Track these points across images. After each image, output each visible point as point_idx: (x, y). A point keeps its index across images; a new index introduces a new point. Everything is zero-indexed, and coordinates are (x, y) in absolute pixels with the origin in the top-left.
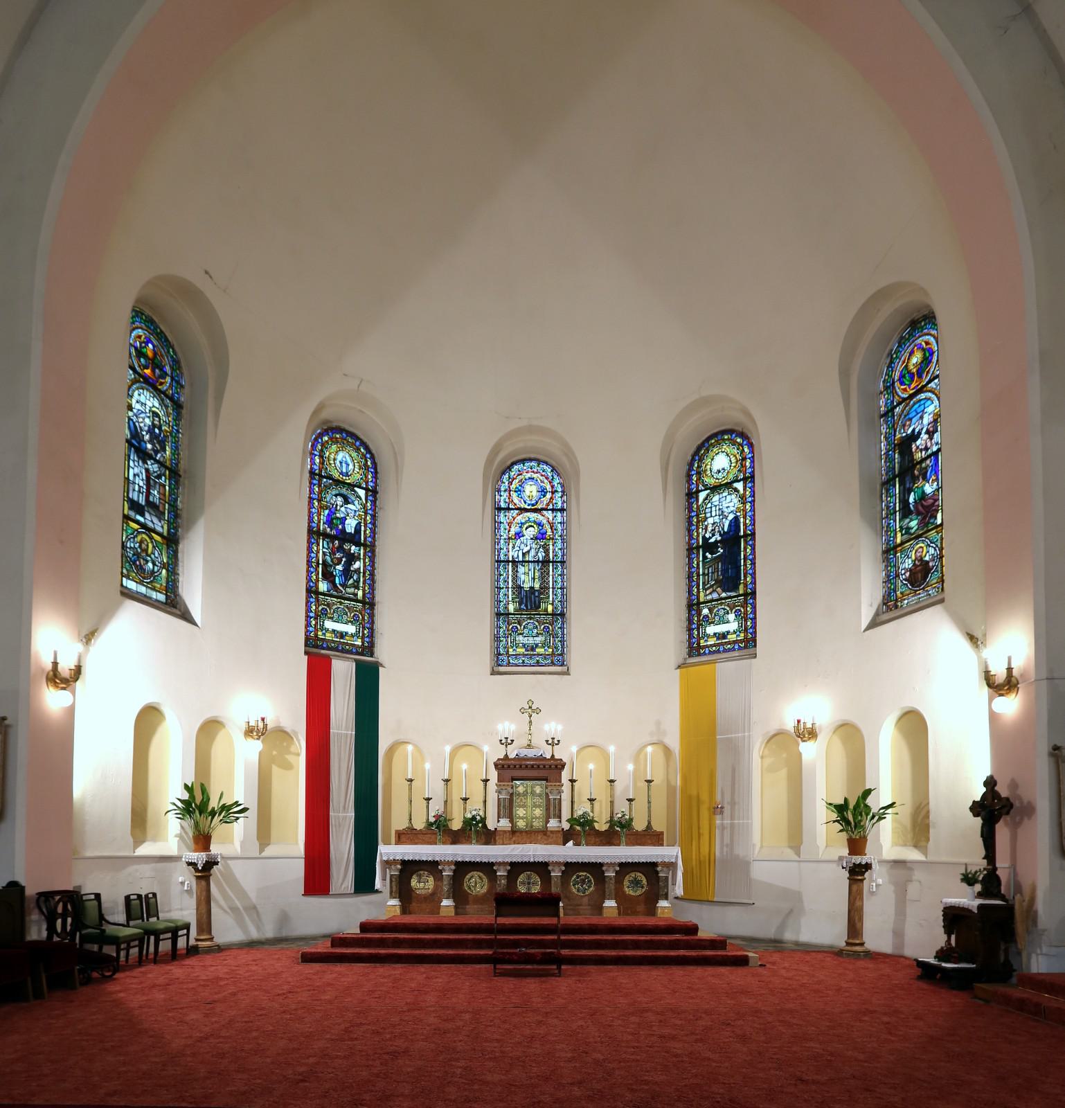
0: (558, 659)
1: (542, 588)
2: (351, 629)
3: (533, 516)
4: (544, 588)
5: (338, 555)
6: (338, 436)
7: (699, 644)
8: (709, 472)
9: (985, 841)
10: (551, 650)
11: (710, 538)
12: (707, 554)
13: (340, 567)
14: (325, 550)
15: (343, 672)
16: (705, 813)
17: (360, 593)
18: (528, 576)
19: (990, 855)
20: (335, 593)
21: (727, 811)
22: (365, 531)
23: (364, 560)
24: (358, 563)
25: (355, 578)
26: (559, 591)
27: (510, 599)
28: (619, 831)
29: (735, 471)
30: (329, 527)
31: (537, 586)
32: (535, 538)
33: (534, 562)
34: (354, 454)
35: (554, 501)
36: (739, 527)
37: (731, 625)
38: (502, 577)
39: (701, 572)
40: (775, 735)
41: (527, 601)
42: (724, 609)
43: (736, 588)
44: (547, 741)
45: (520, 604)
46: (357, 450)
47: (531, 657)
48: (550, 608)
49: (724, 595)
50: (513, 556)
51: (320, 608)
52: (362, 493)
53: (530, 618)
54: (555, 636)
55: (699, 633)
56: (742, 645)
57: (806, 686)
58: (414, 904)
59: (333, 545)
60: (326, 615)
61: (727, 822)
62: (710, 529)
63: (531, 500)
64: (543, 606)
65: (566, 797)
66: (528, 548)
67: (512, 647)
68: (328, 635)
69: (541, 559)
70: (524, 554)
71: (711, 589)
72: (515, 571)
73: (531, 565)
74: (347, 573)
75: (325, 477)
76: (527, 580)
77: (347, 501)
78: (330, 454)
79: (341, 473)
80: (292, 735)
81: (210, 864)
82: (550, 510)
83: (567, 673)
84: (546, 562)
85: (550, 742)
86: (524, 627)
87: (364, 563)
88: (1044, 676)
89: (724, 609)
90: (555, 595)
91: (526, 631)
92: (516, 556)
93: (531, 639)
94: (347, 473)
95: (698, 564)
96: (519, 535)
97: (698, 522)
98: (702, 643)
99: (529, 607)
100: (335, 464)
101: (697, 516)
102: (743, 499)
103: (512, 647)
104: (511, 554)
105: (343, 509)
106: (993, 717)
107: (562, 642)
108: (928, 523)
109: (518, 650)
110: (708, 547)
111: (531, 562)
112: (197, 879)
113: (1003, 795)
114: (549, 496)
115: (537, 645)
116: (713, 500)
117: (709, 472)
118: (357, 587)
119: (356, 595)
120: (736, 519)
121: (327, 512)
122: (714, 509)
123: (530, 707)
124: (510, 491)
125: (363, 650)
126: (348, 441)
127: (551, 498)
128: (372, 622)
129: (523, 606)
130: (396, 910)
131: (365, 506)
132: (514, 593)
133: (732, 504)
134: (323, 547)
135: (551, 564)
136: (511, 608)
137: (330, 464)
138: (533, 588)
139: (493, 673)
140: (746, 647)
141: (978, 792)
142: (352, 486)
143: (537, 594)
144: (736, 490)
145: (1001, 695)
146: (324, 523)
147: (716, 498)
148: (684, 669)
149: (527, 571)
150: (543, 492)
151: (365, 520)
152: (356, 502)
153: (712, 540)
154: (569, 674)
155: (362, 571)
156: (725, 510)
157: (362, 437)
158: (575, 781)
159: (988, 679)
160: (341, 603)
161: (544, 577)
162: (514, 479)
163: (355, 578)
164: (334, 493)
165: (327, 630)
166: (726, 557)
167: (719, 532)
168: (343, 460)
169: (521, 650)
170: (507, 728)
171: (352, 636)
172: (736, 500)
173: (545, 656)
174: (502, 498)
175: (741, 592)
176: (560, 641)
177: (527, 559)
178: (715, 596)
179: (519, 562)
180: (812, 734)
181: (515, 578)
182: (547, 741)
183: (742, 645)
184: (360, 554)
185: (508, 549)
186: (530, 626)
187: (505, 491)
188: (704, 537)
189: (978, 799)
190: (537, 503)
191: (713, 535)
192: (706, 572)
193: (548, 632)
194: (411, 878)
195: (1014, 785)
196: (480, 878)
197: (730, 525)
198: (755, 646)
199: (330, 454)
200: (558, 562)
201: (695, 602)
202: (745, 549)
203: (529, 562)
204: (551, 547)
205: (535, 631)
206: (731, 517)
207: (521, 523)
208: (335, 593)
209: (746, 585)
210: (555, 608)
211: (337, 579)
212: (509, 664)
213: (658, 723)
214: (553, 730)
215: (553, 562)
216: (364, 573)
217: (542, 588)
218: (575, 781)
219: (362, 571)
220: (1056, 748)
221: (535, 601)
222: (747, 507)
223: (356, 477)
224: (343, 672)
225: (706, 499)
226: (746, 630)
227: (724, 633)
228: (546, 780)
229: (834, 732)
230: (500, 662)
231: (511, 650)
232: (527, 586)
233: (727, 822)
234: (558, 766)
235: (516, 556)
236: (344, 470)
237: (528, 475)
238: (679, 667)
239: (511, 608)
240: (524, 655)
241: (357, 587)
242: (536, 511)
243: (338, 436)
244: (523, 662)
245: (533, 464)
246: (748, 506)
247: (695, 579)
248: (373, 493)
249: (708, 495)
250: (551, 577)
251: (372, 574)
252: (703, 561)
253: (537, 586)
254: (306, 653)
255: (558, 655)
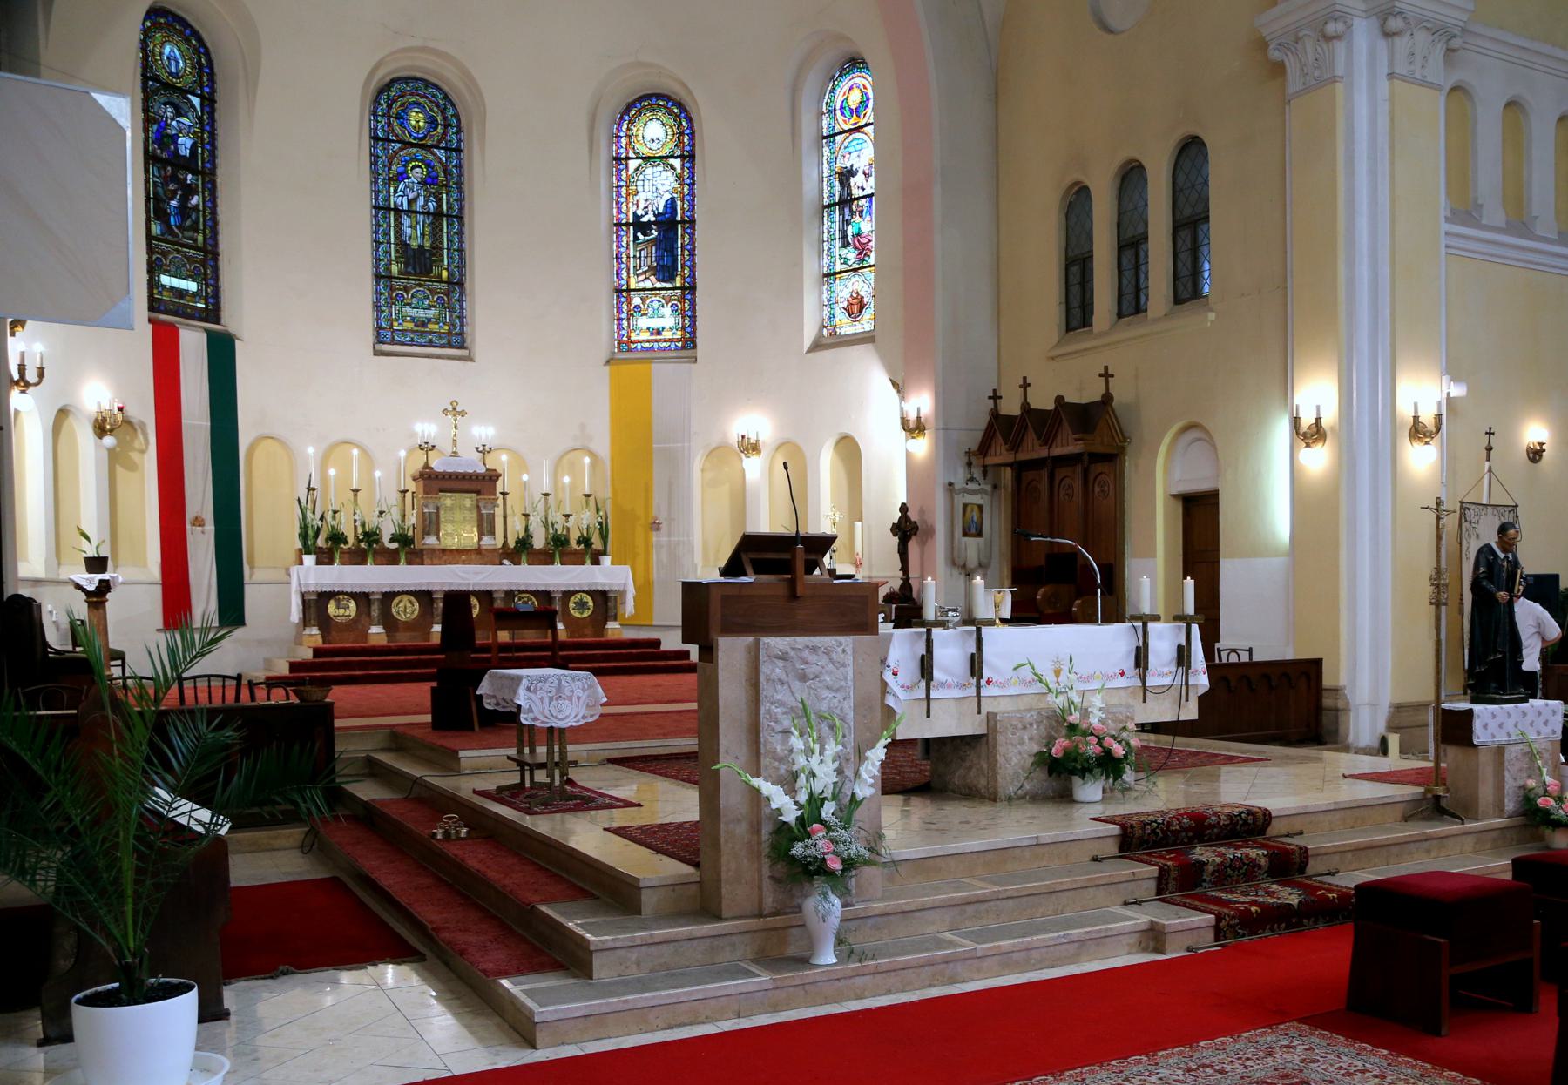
0: (456, 340)
1: (434, 248)
2: (192, 286)
3: (421, 153)
4: (436, 248)
5: (172, 187)
6: (162, 21)
7: (629, 337)
8: (640, 138)
9: (900, 556)
10: (447, 328)
11: (642, 216)
12: (639, 234)
13: (174, 203)
14: (156, 179)
15: (193, 343)
16: (640, 532)
17: (200, 238)
18: (415, 233)
19: (905, 568)
20: (170, 238)
21: (664, 527)
22: (203, 153)
23: (203, 194)
24: (196, 198)
25: (193, 217)
26: (456, 253)
27: (393, 258)
28: (559, 549)
29: (672, 144)
30: (159, 148)
31: (428, 245)
32: (423, 183)
33: (422, 213)
34: (184, 47)
35: (448, 138)
36: (676, 210)
37: (666, 320)
38: (381, 229)
39: (632, 255)
40: (717, 448)
41: (415, 263)
42: (659, 301)
43: (672, 279)
44: (477, 448)
45: (407, 265)
46: (188, 41)
47: (422, 334)
48: (445, 274)
49: (658, 285)
50: (395, 203)
51: (154, 257)
52: (196, 101)
53: (420, 285)
54: (452, 311)
55: (629, 324)
56: (680, 345)
57: (749, 400)
58: (334, 633)
59: (166, 173)
60: (161, 266)
61: (664, 539)
62: (642, 205)
63: (417, 133)
64: (435, 270)
65: (499, 512)
66: (415, 193)
67: (397, 320)
68: (165, 293)
69: (432, 210)
70: (409, 202)
71: (644, 277)
72: (399, 224)
73: (420, 218)
74: (184, 210)
75: (150, 78)
76: (414, 236)
77: (178, 113)
78: (155, 46)
79: (171, 74)
80: (137, 427)
81: (104, 587)
82: (442, 148)
83: (469, 359)
84: (438, 215)
85: (481, 449)
86: (412, 296)
87: (204, 197)
88: (941, 426)
89: (659, 301)
90: (452, 258)
91: (414, 301)
92: (399, 202)
93: (421, 311)
94: (177, 74)
95: (628, 244)
96: (402, 176)
97: (628, 194)
98: (634, 337)
99: (418, 271)
100: (161, 60)
101: (627, 187)
102: (680, 179)
103: (397, 320)
104: (392, 200)
105: (174, 123)
106: (908, 455)
107: (461, 318)
108: (863, 260)
109: (405, 324)
110: (640, 226)
111: (419, 213)
112: (89, 607)
113: (913, 519)
114: (440, 130)
115: (429, 320)
116: (646, 172)
117: (640, 138)
118: (196, 231)
119: (195, 240)
120: (673, 199)
121: (155, 127)
122: (646, 182)
123: (454, 409)
124: (390, 117)
125: (207, 315)
126: (175, 29)
127: (444, 133)
128: (216, 278)
129: (410, 269)
130: (316, 641)
131: (200, 119)
132: (397, 251)
133: (667, 183)
134: (154, 175)
135: (445, 219)
136: (395, 269)
137: (156, 60)
138: (423, 246)
139: (377, 353)
140: (683, 348)
141: (896, 516)
142: (184, 92)
143: (427, 255)
144: (672, 167)
145: (913, 438)
146: (153, 142)
147: (649, 171)
148: (615, 367)
149: (414, 223)
150: (432, 122)
151: (202, 139)
152: (190, 115)
153: (644, 219)
154: (472, 360)
155: (201, 208)
156: (659, 186)
157: (193, 24)
158: (507, 494)
159: (904, 422)
160: (178, 251)
161: (436, 234)
162: (394, 101)
163: (193, 217)
164: (162, 100)
165: (164, 287)
166: (661, 241)
167: (653, 211)
168: (170, 51)
169: (410, 325)
170: (427, 429)
171: (194, 295)
172: (673, 179)
173: (440, 335)
174: (380, 125)
175: (678, 284)
176: (459, 317)
177: (414, 208)
178: (648, 284)
179: (403, 211)
180: (754, 448)
181: (399, 232)
182: (477, 448)
183: (680, 345)
184: (197, 186)
185: (389, 192)
186: (420, 295)
187: (383, 115)
188: (635, 214)
189: (896, 522)
190: (425, 136)
191: (646, 213)
192: (638, 255)
193: (443, 305)
194: (328, 603)
195: (922, 512)
196: (411, 602)
197: (665, 207)
198: (694, 347)
199: (155, 46)
200: (454, 217)
201: (625, 287)
202: (683, 237)
203: (416, 212)
204: (445, 196)
205: (427, 302)
206: (667, 196)
207: (406, 161)
208: (170, 238)
209: (683, 278)
210: (451, 275)
211: (172, 218)
212: (393, 342)
213: (583, 427)
214: (483, 437)
215: (447, 216)
216: (204, 211)
217: (434, 248)
218: (507, 494)
219: (201, 208)
220: (950, 484)
221: (425, 265)
222: (685, 189)
223: (189, 80)
224: (193, 343)
225: (637, 169)
226: (683, 328)
227: (658, 329)
228: (478, 492)
229: (777, 449)
230: (385, 338)
231: (395, 324)
232: (414, 244)
233: (664, 539)
234: (492, 477)
235: (399, 202)
236: (174, 70)
237: (413, 99)
238: (608, 362)
239: (395, 269)
240: (413, 331)
241: (196, 231)
242: (423, 147)
243: (162, 21)
244: (412, 340)
245: (419, 84)
246: (686, 189)
247: (624, 260)
248: (209, 102)
249: (640, 165)
250: (445, 235)
251: (214, 213)
252: (634, 241)
253: (428, 245)
254: (150, 321)
255: (456, 334)
